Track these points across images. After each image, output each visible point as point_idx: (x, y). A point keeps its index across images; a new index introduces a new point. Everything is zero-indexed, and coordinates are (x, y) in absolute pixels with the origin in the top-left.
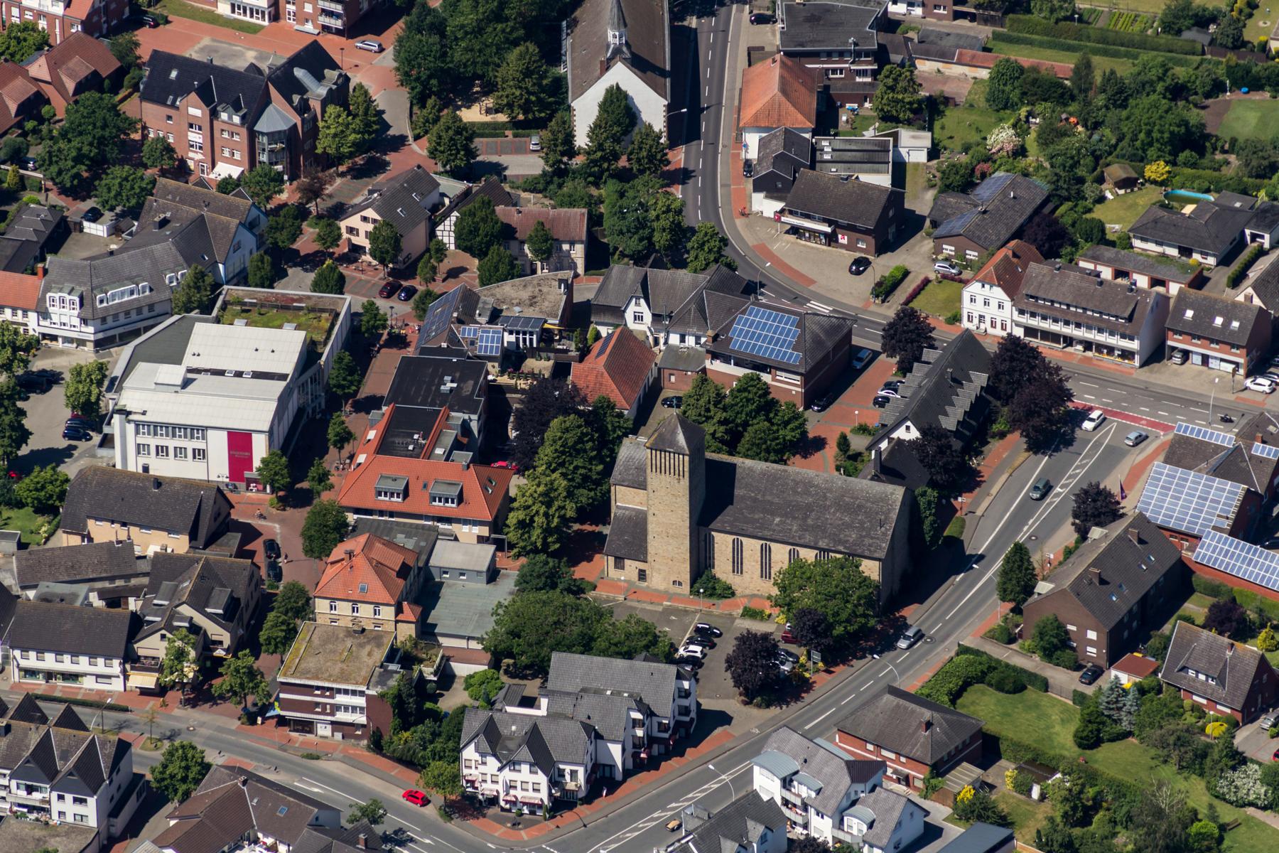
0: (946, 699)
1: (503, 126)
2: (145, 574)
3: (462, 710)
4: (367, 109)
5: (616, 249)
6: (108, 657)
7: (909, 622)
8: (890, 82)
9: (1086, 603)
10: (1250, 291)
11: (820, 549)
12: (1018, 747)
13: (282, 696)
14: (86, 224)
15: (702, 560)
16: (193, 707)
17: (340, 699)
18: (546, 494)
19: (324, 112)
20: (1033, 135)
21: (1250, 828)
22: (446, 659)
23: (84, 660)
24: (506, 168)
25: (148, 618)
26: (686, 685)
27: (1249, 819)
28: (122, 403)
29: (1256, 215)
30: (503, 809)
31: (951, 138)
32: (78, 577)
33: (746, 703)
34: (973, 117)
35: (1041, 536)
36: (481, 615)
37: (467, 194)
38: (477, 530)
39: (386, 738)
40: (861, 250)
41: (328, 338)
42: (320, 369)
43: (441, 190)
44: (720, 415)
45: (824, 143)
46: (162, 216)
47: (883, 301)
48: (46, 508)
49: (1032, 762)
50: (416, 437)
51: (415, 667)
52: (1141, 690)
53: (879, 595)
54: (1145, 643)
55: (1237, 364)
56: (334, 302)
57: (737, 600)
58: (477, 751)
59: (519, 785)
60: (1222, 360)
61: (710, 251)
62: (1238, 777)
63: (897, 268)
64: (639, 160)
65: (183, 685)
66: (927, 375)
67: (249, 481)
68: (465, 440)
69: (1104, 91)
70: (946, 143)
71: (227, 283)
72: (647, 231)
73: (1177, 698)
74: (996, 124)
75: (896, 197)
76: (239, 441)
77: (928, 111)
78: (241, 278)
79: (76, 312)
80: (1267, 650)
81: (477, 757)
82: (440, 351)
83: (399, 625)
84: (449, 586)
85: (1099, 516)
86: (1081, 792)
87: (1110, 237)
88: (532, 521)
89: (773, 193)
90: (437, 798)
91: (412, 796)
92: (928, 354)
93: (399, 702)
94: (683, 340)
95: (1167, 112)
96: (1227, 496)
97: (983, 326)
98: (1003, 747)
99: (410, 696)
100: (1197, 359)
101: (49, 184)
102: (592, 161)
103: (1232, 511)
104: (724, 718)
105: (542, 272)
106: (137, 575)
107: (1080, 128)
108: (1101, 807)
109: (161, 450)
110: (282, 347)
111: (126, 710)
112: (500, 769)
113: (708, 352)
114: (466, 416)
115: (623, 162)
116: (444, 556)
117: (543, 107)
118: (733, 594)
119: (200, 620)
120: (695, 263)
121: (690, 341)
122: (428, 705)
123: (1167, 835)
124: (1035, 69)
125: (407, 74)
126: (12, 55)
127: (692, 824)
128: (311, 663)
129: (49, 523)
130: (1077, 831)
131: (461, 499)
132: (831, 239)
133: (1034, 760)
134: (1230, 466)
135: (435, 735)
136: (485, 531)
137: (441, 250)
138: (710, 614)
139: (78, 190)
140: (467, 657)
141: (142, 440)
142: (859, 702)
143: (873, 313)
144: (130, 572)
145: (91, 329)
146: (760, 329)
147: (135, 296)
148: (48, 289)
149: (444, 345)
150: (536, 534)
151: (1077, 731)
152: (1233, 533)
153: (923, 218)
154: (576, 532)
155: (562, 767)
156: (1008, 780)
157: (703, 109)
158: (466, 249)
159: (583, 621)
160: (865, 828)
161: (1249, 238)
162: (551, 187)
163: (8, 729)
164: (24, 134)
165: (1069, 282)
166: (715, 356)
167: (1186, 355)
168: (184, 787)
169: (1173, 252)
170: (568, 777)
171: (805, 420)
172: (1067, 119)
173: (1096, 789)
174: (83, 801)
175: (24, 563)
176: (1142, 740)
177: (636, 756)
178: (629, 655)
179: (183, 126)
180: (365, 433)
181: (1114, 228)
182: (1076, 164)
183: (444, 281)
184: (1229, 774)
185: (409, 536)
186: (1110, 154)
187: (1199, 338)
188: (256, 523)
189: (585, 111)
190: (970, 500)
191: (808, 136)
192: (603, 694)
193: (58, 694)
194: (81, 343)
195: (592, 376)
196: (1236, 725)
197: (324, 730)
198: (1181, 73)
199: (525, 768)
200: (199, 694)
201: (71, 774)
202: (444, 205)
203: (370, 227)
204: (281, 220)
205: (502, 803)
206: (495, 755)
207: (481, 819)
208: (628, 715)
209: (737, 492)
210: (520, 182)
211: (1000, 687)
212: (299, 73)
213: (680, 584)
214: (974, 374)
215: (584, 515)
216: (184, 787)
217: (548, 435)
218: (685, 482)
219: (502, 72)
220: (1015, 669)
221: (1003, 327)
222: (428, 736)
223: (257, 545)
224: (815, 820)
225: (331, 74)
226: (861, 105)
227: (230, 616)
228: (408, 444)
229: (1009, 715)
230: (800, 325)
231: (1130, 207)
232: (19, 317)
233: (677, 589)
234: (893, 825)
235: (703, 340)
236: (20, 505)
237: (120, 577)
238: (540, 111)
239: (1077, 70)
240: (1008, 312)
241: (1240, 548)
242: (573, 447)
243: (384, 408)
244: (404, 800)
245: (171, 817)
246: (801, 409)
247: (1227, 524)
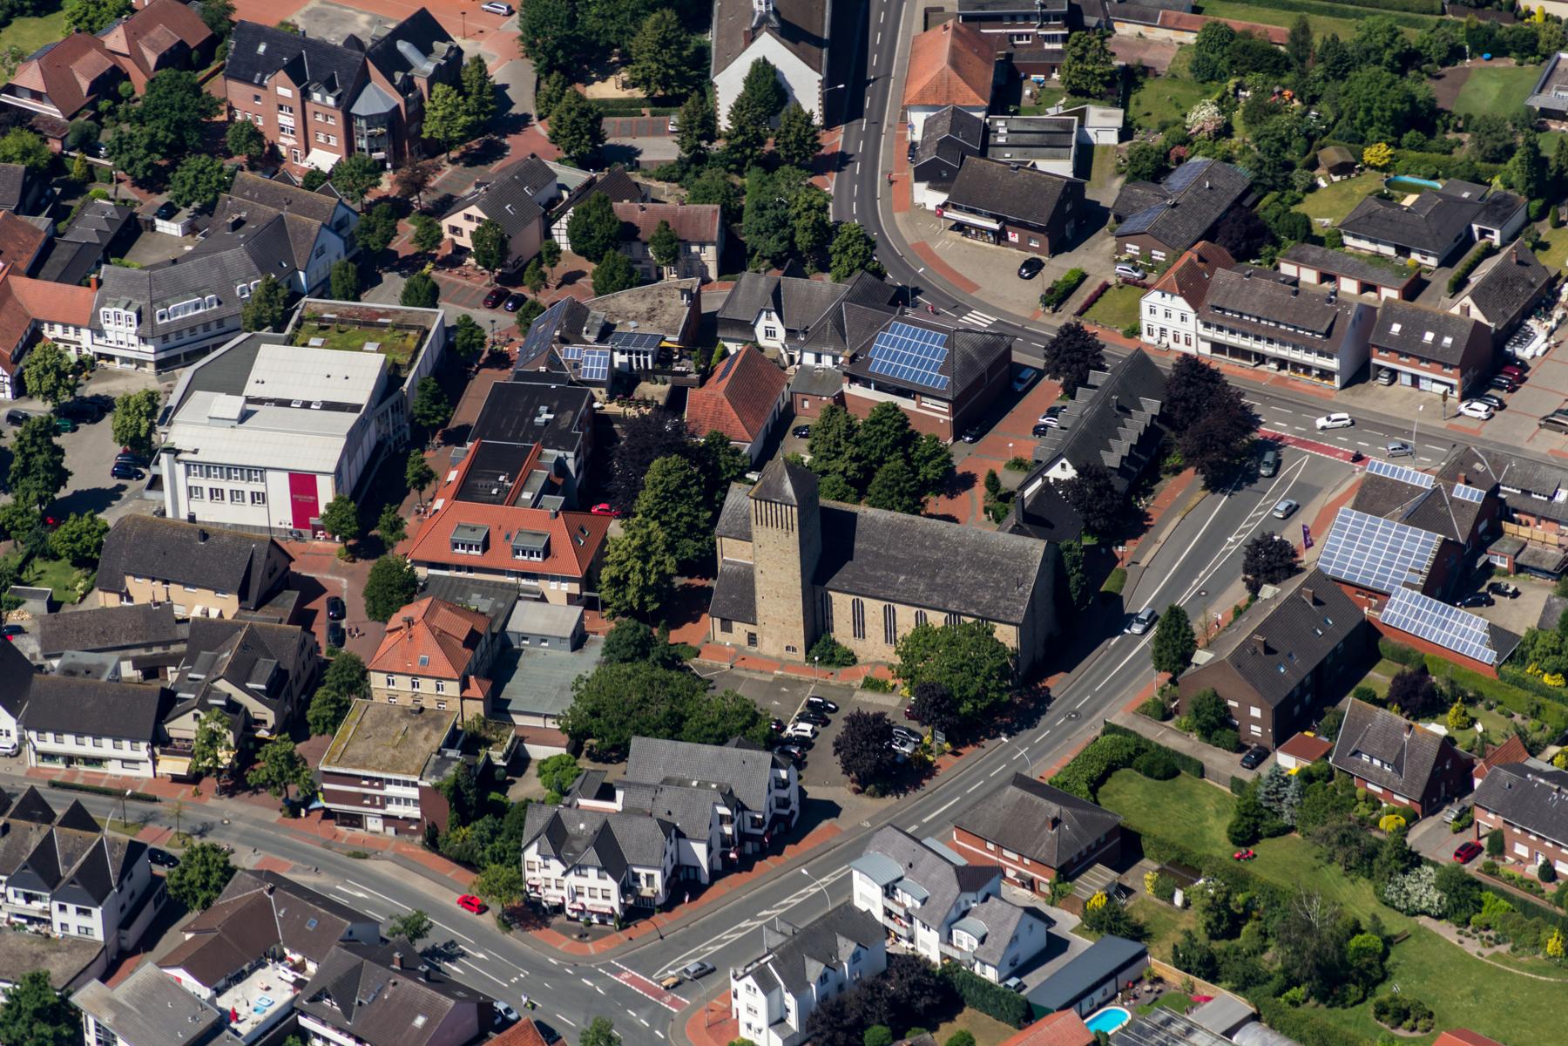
0: (1085, 787)
1: (640, 103)
2: (184, 641)
3: (526, 803)
4: (481, 87)
5: (754, 250)
6: (135, 740)
7: (1052, 694)
8: (1078, 51)
9: (1249, 676)
10: (1468, 301)
11: (950, 613)
12: (1162, 844)
13: (326, 786)
14: (158, 222)
15: (820, 622)
16: (231, 795)
17: (391, 790)
18: (642, 547)
19: (430, 91)
20: (1238, 114)
21: (1420, 940)
22: (519, 740)
23: (107, 743)
24: (639, 153)
25: (180, 695)
26: (783, 774)
27: (1421, 930)
28: (171, 440)
29: (1486, 208)
30: (569, 918)
31: (1148, 114)
32: (110, 645)
33: (857, 792)
34: (1174, 90)
35: (1207, 595)
36: (562, 689)
37: (590, 184)
38: (565, 587)
39: (442, 835)
40: (1034, 249)
41: (413, 361)
42: (403, 398)
43: (559, 181)
44: (851, 451)
45: (999, 124)
46: (236, 217)
47: (1054, 311)
48: (85, 561)
49: (1176, 863)
50: (501, 478)
51: (483, 751)
52: (1307, 777)
53: (1017, 664)
54: (1319, 719)
55: (1451, 386)
56: (425, 316)
57: (858, 668)
58: (538, 853)
59: (586, 892)
60: (1434, 381)
61: (855, 255)
62: (1410, 883)
63: (1073, 272)
64: (786, 145)
65: (220, 771)
66: (1091, 402)
67: (315, 529)
68: (560, 481)
69: (1323, 60)
70: (1142, 121)
71: (310, 293)
72: (788, 231)
73: (1350, 786)
74: (1196, 101)
75: (1073, 190)
76: (302, 484)
77: (1123, 84)
78: (322, 289)
79: (134, 329)
80: (1459, 728)
81: (539, 859)
82: (537, 376)
83: (466, 702)
84: (529, 654)
85: (1272, 571)
86: (1227, 900)
87: (1317, 232)
88: (627, 577)
89: (936, 183)
90: (496, 907)
91: (467, 902)
92: (1096, 377)
93: (456, 794)
94: (818, 360)
95: (1388, 87)
96: (1421, 546)
97: (1165, 340)
98: (1145, 843)
99: (469, 787)
100: (1406, 380)
101: (121, 174)
102: (733, 147)
103: (1427, 563)
104: (830, 810)
105: (670, 277)
106: (177, 642)
107: (1296, 103)
108: (1251, 916)
109: (216, 494)
110: (354, 373)
111: (153, 800)
112: (565, 874)
113: (845, 374)
114: (561, 454)
115: (769, 146)
116: (525, 619)
117: (684, 81)
118: (855, 661)
119: (239, 696)
120: (839, 269)
121: (827, 361)
122: (494, 796)
123: (1316, 954)
124: (1247, 34)
125: (532, 45)
126: (91, 22)
127: (774, 940)
128: (359, 749)
129: (87, 578)
130: (1219, 946)
131: (547, 552)
132: (1000, 237)
133: (1179, 861)
134: (1426, 511)
135: (495, 833)
136: (575, 588)
137: (555, 252)
138: (826, 685)
139: (152, 181)
140: (543, 738)
141: (193, 481)
142: (987, 790)
143: (1042, 325)
144: (168, 638)
145: (151, 349)
146: (907, 347)
147: (201, 311)
148: (102, 303)
149: (543, 369)
150: (632, 592)
151: (1231, 826)
152: (1428, 590)
153: (1106, 211)
154: (674, 592)
155: (636, 870)
156: (1148, 885)
157: (870, 82)
158: (579, 252)
159: (675, 697)
160: (975, 943)
161: (1477, 235)
162: (688, 176)
163: (6, 828)
164: (97, 117)
165: (1261, 291)
166: (853, 379)
167: (1394, 375)
168: (205, 895)
169: (1389, 251)
170: (643, 882)
171: (950, 456)
172: (1280, 93)
173: (1248, 894)
174: (87, 913)
175: (48, 628)
176: (1306, 835)
177: (724, 855)
178: (721, 740)
179: (270, 106)
180: (447, 474)
181: (1323, 223)
182: (1285, 145)
183: (558, 287)
184: (1399, 878)
185: (485, 596)
186: (1325, 133)
187: (1407, 356)
188: (322, 577)
189: (729, 85)
190: (1133, 548)
191: (980, 115)
192: (693, 783)
193: (78, 781)
194: (141, 363)
195: (712, 408)
196: (1413, 819)
197: (374, 824)
198: (1413, 36)
199: (592, 872)
200: (236, 782)
201: (73, 882)
202: (561, 198)
203: (473, 226)
204: (373, 219)
205: (569, 912)
206: (558, 858)
207: (545, 930)
208: (714, 810)
209: (857, 545)
210: (653, 170)
211: (1149, 773)
212: (403, 46)
213: (794, 650)
214: (1145, 401)
215: (685, 568)
216: (205, 895)
217: (648, 478)
218: (795, 536)
219: (639, 39)
220: (1167, 751)
221: (1188, 343)
222: (487, 834)
223: (320, 604)
224: (921, 933)
225: (441, 47)
226: (1048, 76)
227: (275, 691)
228: (492, 487)
229: (1157, 806)
230: (948, 344)
231: (1345, 197)
232: (71, 335)
233: (790, 655)
234: (1007, 940)
235: (841, 360)
236: (55, 557)
237: (158, 644)
238: (680, 87)
239: (1293, 36)
240: (1193, 325)
241: (1434, 608)
242: (675, 492)
243: (469, 444)
244: (459, 907)
245: (186, 929)
246: (950, 441)
247: (1419, 580)
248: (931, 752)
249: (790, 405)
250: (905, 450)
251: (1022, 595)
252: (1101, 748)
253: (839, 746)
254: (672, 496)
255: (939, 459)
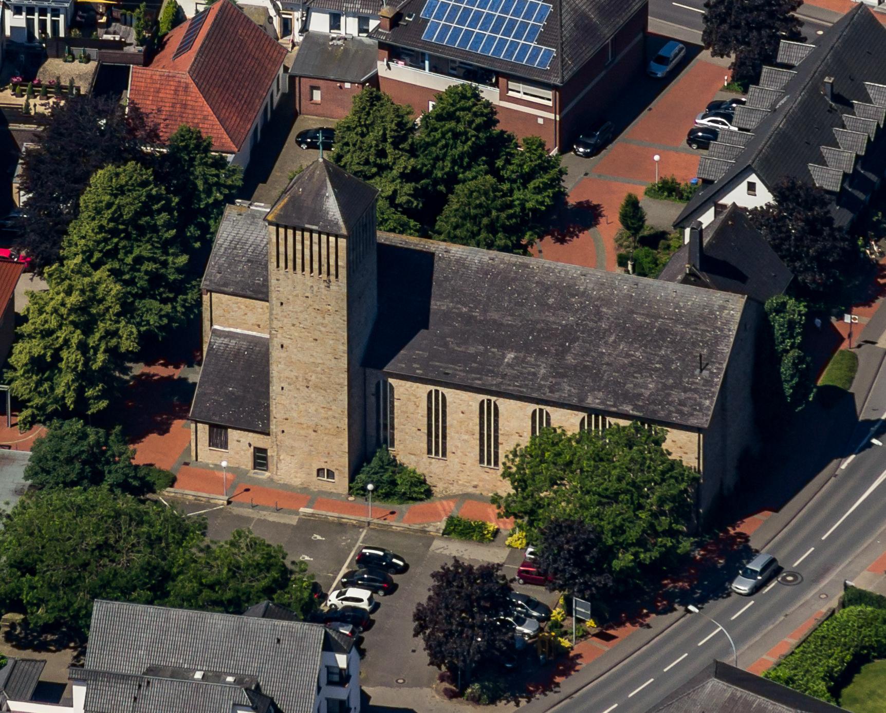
0: (822, 686)
7: (753, 545)
11: (590, 411)
15: (372, 431)
18: (82, 309)
26: (342, 660)
44: (405, 163)
53: (697, 496)
57: (436, 504)
66: (788, 89)
88: (57, 358)
94: (335, 23)
113: (382, 46)
118: (429, 493)
121: (350, 26)
138: (385, 530)
142: (662, 692)
150: (64, 382)
159: (152, 542)
166: (395, 54)
190: (865, 320)
213: (331, 474)
215: (152, 347)
217: (87, 199)
218: (340, 286)
233: (325, 484)
235: (373, 24)
248: (564, 634)
249: (289, 98)
250: (491, 163)
251: (708, 382)
252: (844, 627)
253: (422, 620)
254: (124, 229)
255: (546, 178)
